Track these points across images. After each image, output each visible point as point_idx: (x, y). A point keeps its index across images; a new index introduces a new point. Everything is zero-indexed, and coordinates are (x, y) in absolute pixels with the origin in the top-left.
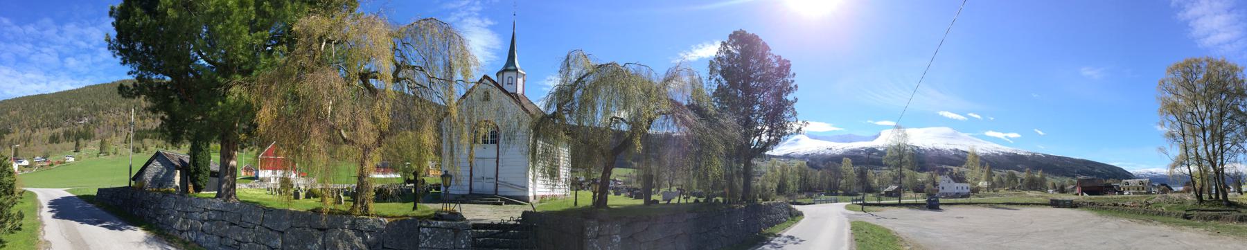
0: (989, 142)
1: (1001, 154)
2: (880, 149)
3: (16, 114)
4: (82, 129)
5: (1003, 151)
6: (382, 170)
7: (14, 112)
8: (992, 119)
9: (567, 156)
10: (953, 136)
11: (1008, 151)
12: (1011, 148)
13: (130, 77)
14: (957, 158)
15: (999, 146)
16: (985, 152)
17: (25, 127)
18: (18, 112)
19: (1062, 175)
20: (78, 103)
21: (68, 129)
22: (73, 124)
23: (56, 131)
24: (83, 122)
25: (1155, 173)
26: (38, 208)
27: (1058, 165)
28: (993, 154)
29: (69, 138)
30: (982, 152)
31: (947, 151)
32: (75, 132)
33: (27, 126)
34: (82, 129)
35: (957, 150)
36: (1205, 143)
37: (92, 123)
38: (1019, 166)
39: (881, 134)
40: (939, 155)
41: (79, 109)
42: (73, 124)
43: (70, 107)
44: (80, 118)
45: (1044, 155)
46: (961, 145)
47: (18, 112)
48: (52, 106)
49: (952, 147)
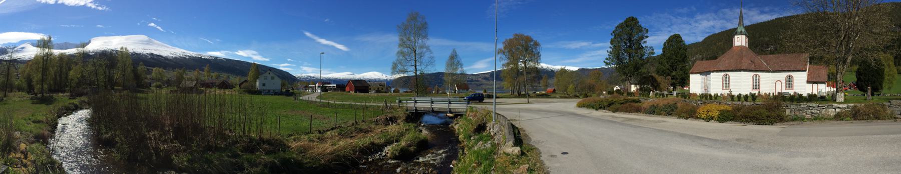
1: (188, 57)
2: (91, 54)
5: (189, 55)
6: (117, 75)
7: (720, 43)
9: (815, 66)
10: (148, 43)
11: (194, 55)
14: (153, 61)
15: (184, 51)
16: (174, 56)
18: (722, 43)
20: (767, 34)
22: (762, 50)
24: (769, 49)
25: (313, 77)
26: (429, 99)
27: (238, 68)
28: (181, 57)
30: (172, 55)
31: (145, 55)
35: (152, 54)
37: (776, 50)
39: (92, 41)
41: (767, 39)
42: (762, 50)
43: (760, 37)
46: (155, 50)
47: (722, 43)
49: (148, 52)
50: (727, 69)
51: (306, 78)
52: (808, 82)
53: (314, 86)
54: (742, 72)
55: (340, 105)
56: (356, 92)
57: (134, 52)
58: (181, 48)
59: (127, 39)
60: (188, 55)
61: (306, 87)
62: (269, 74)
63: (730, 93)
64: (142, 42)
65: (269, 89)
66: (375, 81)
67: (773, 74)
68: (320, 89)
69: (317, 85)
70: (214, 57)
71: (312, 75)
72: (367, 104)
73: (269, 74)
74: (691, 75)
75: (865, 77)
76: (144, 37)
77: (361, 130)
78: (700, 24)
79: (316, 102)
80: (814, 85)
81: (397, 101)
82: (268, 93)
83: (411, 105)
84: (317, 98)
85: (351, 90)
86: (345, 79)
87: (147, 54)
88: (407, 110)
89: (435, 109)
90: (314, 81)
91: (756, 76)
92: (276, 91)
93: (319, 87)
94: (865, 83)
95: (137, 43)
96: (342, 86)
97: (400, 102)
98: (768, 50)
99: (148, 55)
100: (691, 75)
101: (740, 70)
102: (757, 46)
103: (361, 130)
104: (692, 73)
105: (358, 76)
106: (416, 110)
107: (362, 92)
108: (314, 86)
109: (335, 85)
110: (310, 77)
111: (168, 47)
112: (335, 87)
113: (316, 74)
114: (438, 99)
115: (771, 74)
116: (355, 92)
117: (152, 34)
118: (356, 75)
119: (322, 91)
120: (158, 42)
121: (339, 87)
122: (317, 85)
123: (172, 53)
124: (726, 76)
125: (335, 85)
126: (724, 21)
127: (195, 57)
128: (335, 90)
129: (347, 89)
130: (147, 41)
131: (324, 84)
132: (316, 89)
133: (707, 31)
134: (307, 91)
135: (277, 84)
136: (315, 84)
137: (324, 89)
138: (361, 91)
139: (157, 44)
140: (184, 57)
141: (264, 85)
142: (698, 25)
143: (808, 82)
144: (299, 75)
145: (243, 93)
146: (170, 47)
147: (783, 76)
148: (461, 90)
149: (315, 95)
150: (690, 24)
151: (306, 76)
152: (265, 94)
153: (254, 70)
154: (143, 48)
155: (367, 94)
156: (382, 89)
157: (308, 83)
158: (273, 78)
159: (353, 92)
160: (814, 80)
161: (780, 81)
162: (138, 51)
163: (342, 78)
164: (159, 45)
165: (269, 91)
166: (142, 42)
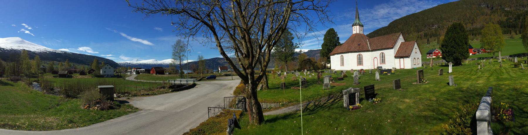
0: (41, 46)
3: (401, 27)
4: (434, 32)
5: (49, 51)
8: (37, 27)
10: (22, 42)
11: (51, 51)
12: (52, 49)
13: (186, 129)
16: (39, 51)
17: (405, 33)
19: (83, 64)
21: (426, 32)
22: (429, 29)
23: (420, 33)
24: (434, 27)
25: (129, 63)
26: (180, 80)
28: (43, 52)
29: (427, 37)
30: (38, 51)
31: (19, 51)
32: (430, 33)
33: (406, 32)
34: (434, 32)
36: (256, 98)
37: (439, 28)
38: (58, 59)
40: (16, 53)
41: (432, 20)
42: (429, 29)
43: (427, 20)
44: (433, 25)
45: (72, 53)
48: (418, 19)
49: (22, 48)
50: (342, 51)
51: (125, 64)
52: (396, 57)
53: (131, 70)
54: (350, 54)
55: (146, 82)
56: (156, 74)
57: (12, 49)
58: (43, 46)
59: (7, 40)
60: (48, 50)
61: (126, 71)
62: (108, 66)
63: (255, 73)
64: (17, 42)
65: (108, 74)
66: (168, 66)
67: (372, 52)
68: (135, 72)
69: (133, 70)
70: (64, 52)
71: (128, 62)
72: (156, 82)
73: (108, 66)
74: (331, 56)
75: (445, 49)
76: (18, 39)
77: (151, 90)
78: (378, 12)
79: (135, 81)
80: (401, 59)
81: (168, 81)
82: (108, 76)
83: (173, 82)
84: (134, 78)
85: (153, 73)
86: (151, 64)
87: (21, 50)
88: (171, 84)
89: (182, 84)
90: (131, 66)
91: (360, 55)
92: (112, 75)
93: (134, 71)
94: (446, 54)
95: (14, 43)
96: (149, 69)
97: (169, 81)
98: (433, 28)
99: (22, 51)
100: (331, 56)
101: (348, 52)
102: (426, 26)
103: (151, 90)
104: (331, 55)
105: (160, 62)
106: (175, 84)
107: (160, 74)
108: (131, 70)
109: (144, 70)
110: (127, 63)
111: (36, 45)
112: (144, 70)
113: (131, 61)
114: (183, 80)
115: (370, 53)
116: (156, 74)
117: (24, 37)
118: (158, 61)
119: (136, 74)
120: (28, 42)
121: (147, 71)
122: (133, 70)
123: (38, 49)
124: (360, 55)
125: (144, 70)
126: (395, 8)
127: (52, 52)
128: (144, 72)
129: (151, 72)
130: (20, 41)
131: (137, 67)
132: (132, 73)
133: (385, 16)
134: (127, 73)
135: (111, 71)
136: (132, 69)
137: (138, 73)
138: (160, 74)
139: (27, 43)
140: (46, 52)
141: (105, 72)
142: (378, 13)
143: (396, 57)
144: (120, 62)
145: (94, 77)
146: (36, 45)
147: (377, 53)
148: (223, 71)
149: (132, 76)
150: (372, 13)
151: (124, 63)
152: (106, 77)
153: (96, 62)
154: (18, 46)
155: (163, 75)
156: (173, 72)
157: (128, 67)
158: (110, 68)
159: (155, 74)
160: (401, 55)
161: (375, 58)
162: (15, 48)
163: (149, 63)
164: (28, 44)
165: (108, 75)
166: (17, 42)
